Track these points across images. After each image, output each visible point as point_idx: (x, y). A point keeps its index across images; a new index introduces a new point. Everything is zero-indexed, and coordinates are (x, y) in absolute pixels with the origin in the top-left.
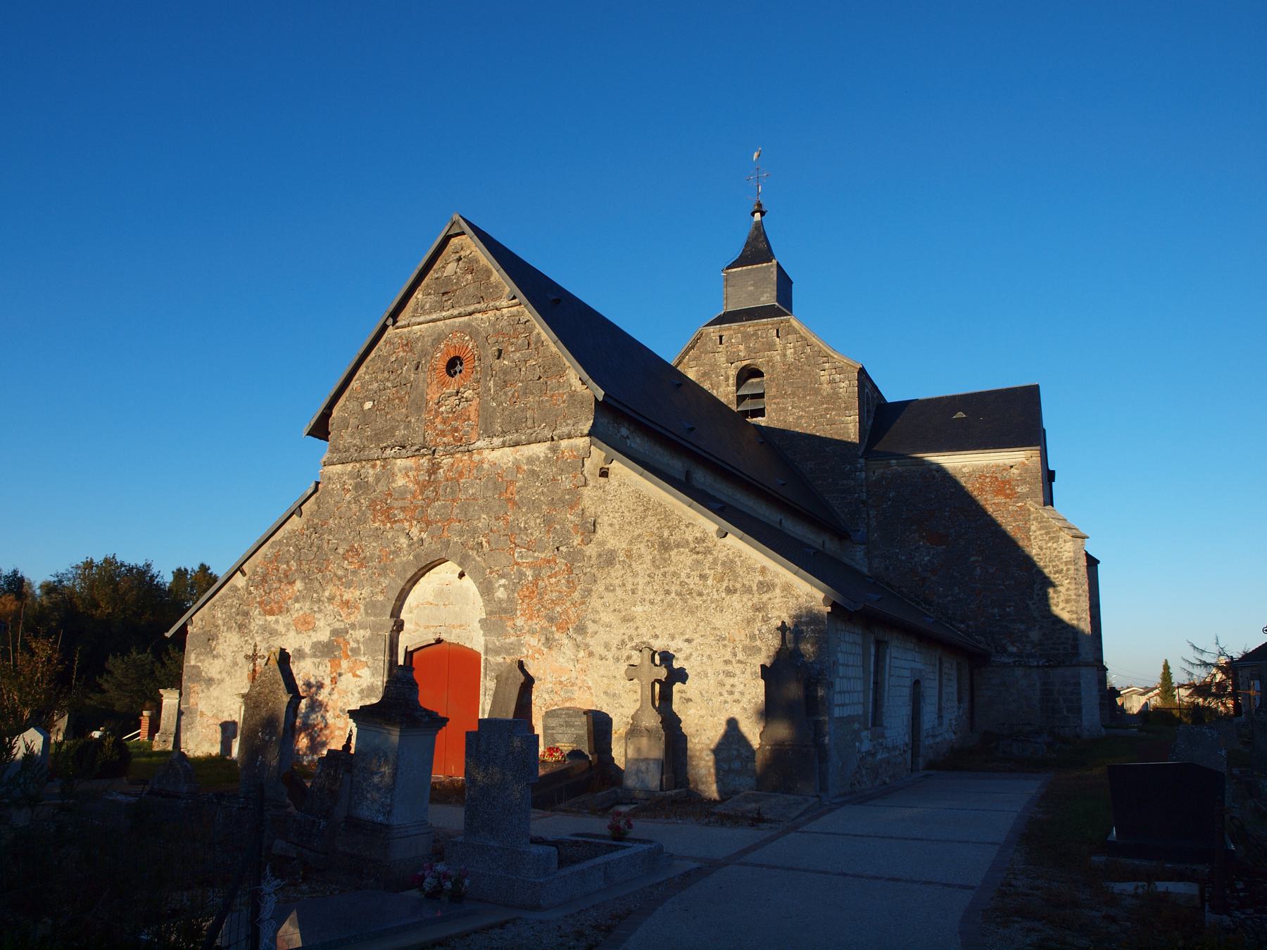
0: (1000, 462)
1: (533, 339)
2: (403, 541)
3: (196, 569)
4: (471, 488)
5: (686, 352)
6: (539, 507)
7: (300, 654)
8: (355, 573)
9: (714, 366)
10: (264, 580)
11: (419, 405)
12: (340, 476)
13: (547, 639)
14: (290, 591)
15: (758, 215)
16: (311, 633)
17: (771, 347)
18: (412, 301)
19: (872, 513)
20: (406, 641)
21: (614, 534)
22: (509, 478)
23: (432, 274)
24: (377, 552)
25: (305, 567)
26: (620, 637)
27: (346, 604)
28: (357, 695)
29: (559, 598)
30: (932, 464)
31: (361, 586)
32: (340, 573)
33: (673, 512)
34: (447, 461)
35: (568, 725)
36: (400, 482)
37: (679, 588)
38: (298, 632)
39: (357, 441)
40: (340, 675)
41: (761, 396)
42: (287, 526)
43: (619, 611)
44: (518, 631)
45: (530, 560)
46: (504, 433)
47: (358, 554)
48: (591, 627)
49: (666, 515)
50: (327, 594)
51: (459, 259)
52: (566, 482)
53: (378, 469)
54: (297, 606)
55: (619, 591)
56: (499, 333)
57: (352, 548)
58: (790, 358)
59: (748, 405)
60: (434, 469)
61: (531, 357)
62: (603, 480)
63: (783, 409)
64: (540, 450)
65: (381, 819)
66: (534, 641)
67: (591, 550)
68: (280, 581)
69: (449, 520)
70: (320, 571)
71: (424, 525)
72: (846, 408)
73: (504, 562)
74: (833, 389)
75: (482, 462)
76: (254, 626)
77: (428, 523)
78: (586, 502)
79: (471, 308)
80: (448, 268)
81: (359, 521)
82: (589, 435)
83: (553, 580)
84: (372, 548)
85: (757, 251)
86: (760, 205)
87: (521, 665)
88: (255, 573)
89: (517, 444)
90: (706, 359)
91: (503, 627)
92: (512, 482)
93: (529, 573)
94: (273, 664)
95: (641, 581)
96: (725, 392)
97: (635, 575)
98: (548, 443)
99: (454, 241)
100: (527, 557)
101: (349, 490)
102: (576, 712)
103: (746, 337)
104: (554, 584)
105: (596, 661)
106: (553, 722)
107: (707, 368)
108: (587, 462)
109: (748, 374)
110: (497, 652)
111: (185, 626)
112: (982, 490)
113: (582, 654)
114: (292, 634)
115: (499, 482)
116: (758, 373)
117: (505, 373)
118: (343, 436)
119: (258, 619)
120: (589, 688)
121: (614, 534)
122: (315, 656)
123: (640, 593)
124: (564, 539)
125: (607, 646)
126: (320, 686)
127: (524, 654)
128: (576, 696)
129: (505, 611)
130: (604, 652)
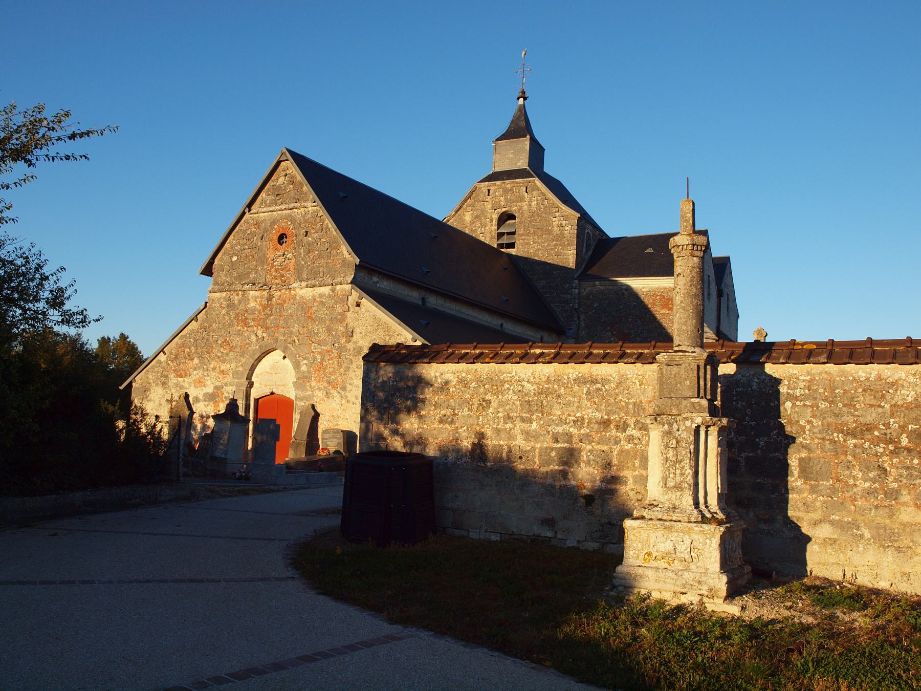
1: (324, 227)
2: (254, 338)
3: (117, 337)
5: (465, 201)
6: (325, 322)
7: (197, 399)
8: (227, 354)
9: (483, 211)
10: (176, 357)
11: (263, 261)
12: (219, 299)
14: (191, 364)
15: (521, 100)
17: (522, 199)
18: (260, 198)
19: (582, 317)
20: (255, 394)
21: (362, 338)
23: (270, 183)
25: (199, 351)
27: (222, 372)
29: (334, 371)
32: (219, 354)
34: (277, 294)
35: (334, 437)
36: (252, 304)
38: (196, 387)
39: (228, 279)
41: (514, 233)
46: (308, 279)
48: (349, 387)
49: (388, 329)
53: (240, 296)
54: (195, 372)
56: (306, 221)
57: (225, 341)
58: (534, 208)
59: (505, 240)
60: (270, 298)
62: (357, 308)
63: (527, 244)
64: (326, 290)
65: (223, 456)
67: (350, 346)
68: (185, 358)
72: (568, 245)
73: (306, 351)
75: (296, 295)
76: (171, 384)
77: (267, 328)
78: (349, 320)
79: (292, 206)
80: (280, 180)
82: (351, 283)
84: (236, 341)
85: (520, 128)
86: (523, 92)
87: (313, 407)
88: (171, 353)
89: (314, 286)
90: (478, 205)
91: (305, 386)
92: (311, 307)
93: (319, 357)
94: (182, 398)
96: (487, 234)
99: (283, 164)
102: (337, 431)
103: (506, 191)
105: (351, 405)
106: (326, 436)
107: (479, 212)
108: (350, 298)
109: (506, 217)
110: (301, 400)
111: (131, 383)
113: (344, 401)
114: (192, 388)
115: (304, 307)
116: (513, 217)
117: (309, 245)
119: (173, 380)
121: (362, 338)
122: (205, 400)
127: (315, 401)
129: (306, 377)
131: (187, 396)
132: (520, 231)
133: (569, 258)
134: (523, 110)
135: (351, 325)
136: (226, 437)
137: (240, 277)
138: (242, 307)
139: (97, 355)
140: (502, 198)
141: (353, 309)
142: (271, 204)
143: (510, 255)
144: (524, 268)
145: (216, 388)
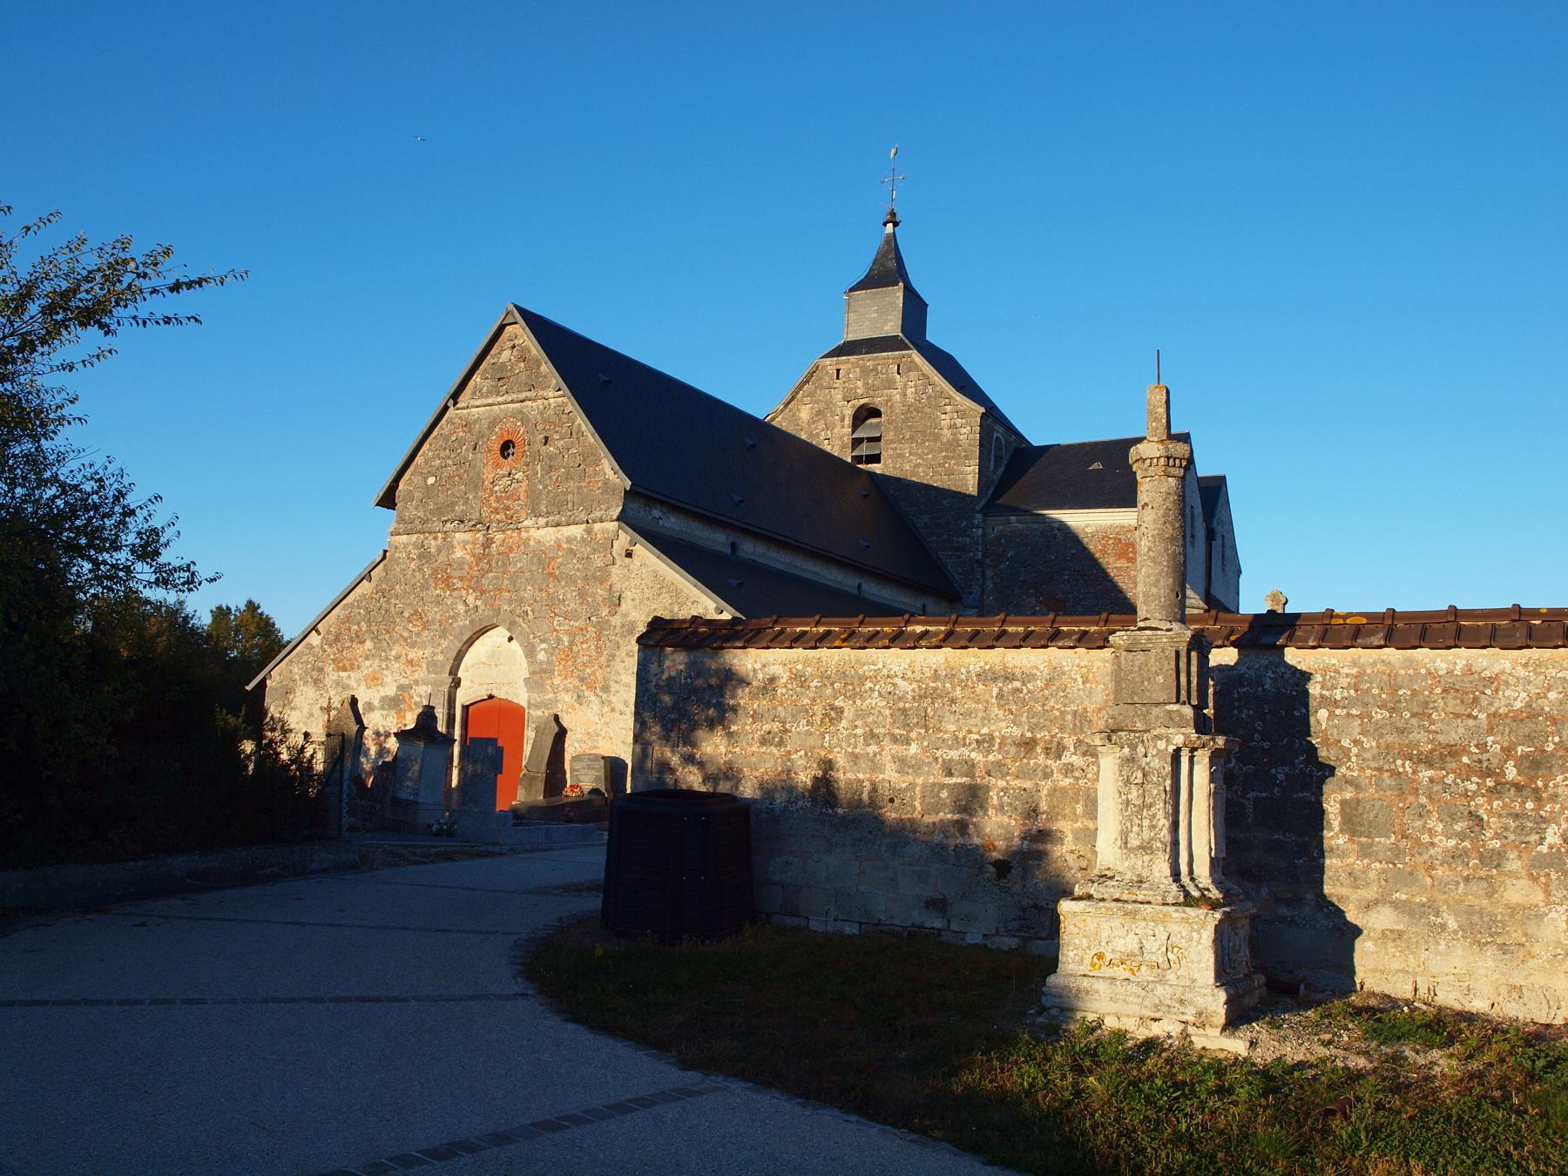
0: (1125, 523)
1: (575, 428)
2: (461, 607)
3: (242, 607)
4: (520, 562)
7: (370, 707)
8: (418, 634)
9: (829, 403)
10: (337, 639)
11: (476, 484)
12: (406, 545)
15: (890, 225)
17: (891, 385)
18: (471, 383)
19: (989, 573)
20: (462, 697)
23: (489, 360)
25: (374, 628)
27: (411, 662)
30: (1054, 521)
32: (406, 634)
34: (499, 537)
35: (590, 767)
36: (459, 553)
38: (368, 687)
39: (421, 514)
41: (878, 439)
48: (614, 687)
49: (677, 593)
52: (598, 560)
56: (545, 421)
58: (911, 398)
59: (864, 450)
60: (488, 543)
64: (577, 531)
67: (616, 621)
68: (352, 641)
69: (501, 590)
72: (966, 457)
73: (545, 628)
74: (954, 435)
75: (528, 539)
76: (327, 681)
77: (483, 592)
78: (614, 579)
79: (522, 396)
80: (503, 355)
82: (618, 519)
84: (433, 613)
85: (888, 270)
86: (893, 214)
87: (556, 718)
88: (329, 632)
89: (558, 525)
93: (566, 639)
94: (347, 704)
96: (835, 440)
102: (595, 758)
103: (865, 372)
104: (586, 649)
105: (616, 715)
106: (578, 765)
107: (822, 406)
108: (616, 544)
109: (866, 413)
110: (538, 707)
111: (264, 680)
112: (1104, 552)
114: (363, 688)
116: (876, 413)
118: (409, 506)
119: (331, 675)
124: (595, 610)
127: (558, 709)
129: (545, 671)
131: (354, 701)
132: (889, 436)
133: (967, 478)
134: (892, 241)
135: (617, 587)
136: (416, 768)
137: (439, 511)
138: (442, 558)
139: (209, 636)
140: (860, 384)
141: (622, 561)
142: (489, 394)
143: (872, 475)
144: (896, 497)
145: (401, 688)
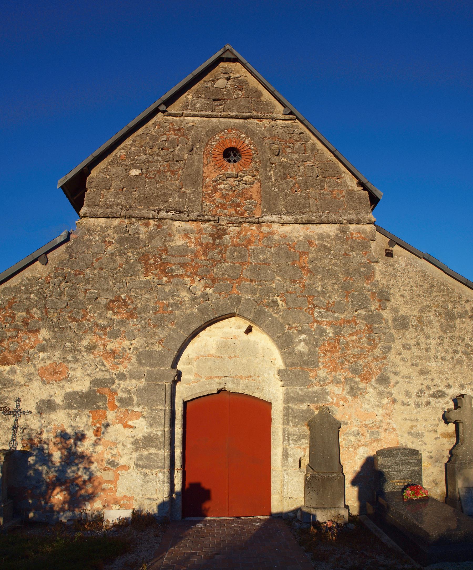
8: (122, 323)
11: (195, 179)
12: (103, 229)
13: (352, 388)
16: (64, 383)
20: (183, 392)
22: (302, 250)
24: (152, 304)
25: (54, 316)
26: (419, 387)
27: (113, 353)
28: (129, 446)
31: (130, 336)
32: (102, 322)
33: (454, 291)
34: (233, 229)
36: (179, 241)
37: (464, 349)
40: (107, 425)
42: (27, 273)
43: (417, 365)
44: (323, 382)
45: (331, 319)
47: (125, 304)
48: (393, 379)
49: (450, 293)
50: (85, 343)
51: (228, 79)
53: (151, 228)
54: (41, 355)
55: (415, 350)
61: (308, 159)
66: (338, 390)
70: (74, 320)
71: (209, 282)
73: (304, 319)
78: (378, 276)
81: (126, 273)
83: (354, 338)
84: (143, 299)
89: (309, 222)
95: (433, 343)
97: (427, 337)
98: (337, 226)
100: (327, 317)
101: (111, 243)
105: (398, 406)
113: (385, 401)
115: (289, 252)
120: (394, 430)
121: (406, 303)
122: (69, 407)
123: (433, 351)
125: (408, 394)
126: (80, 437)
128: (382, 436)
129: (307, 363)
130: (406, 400)
